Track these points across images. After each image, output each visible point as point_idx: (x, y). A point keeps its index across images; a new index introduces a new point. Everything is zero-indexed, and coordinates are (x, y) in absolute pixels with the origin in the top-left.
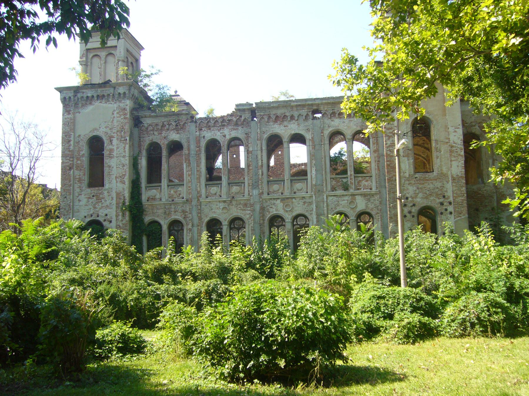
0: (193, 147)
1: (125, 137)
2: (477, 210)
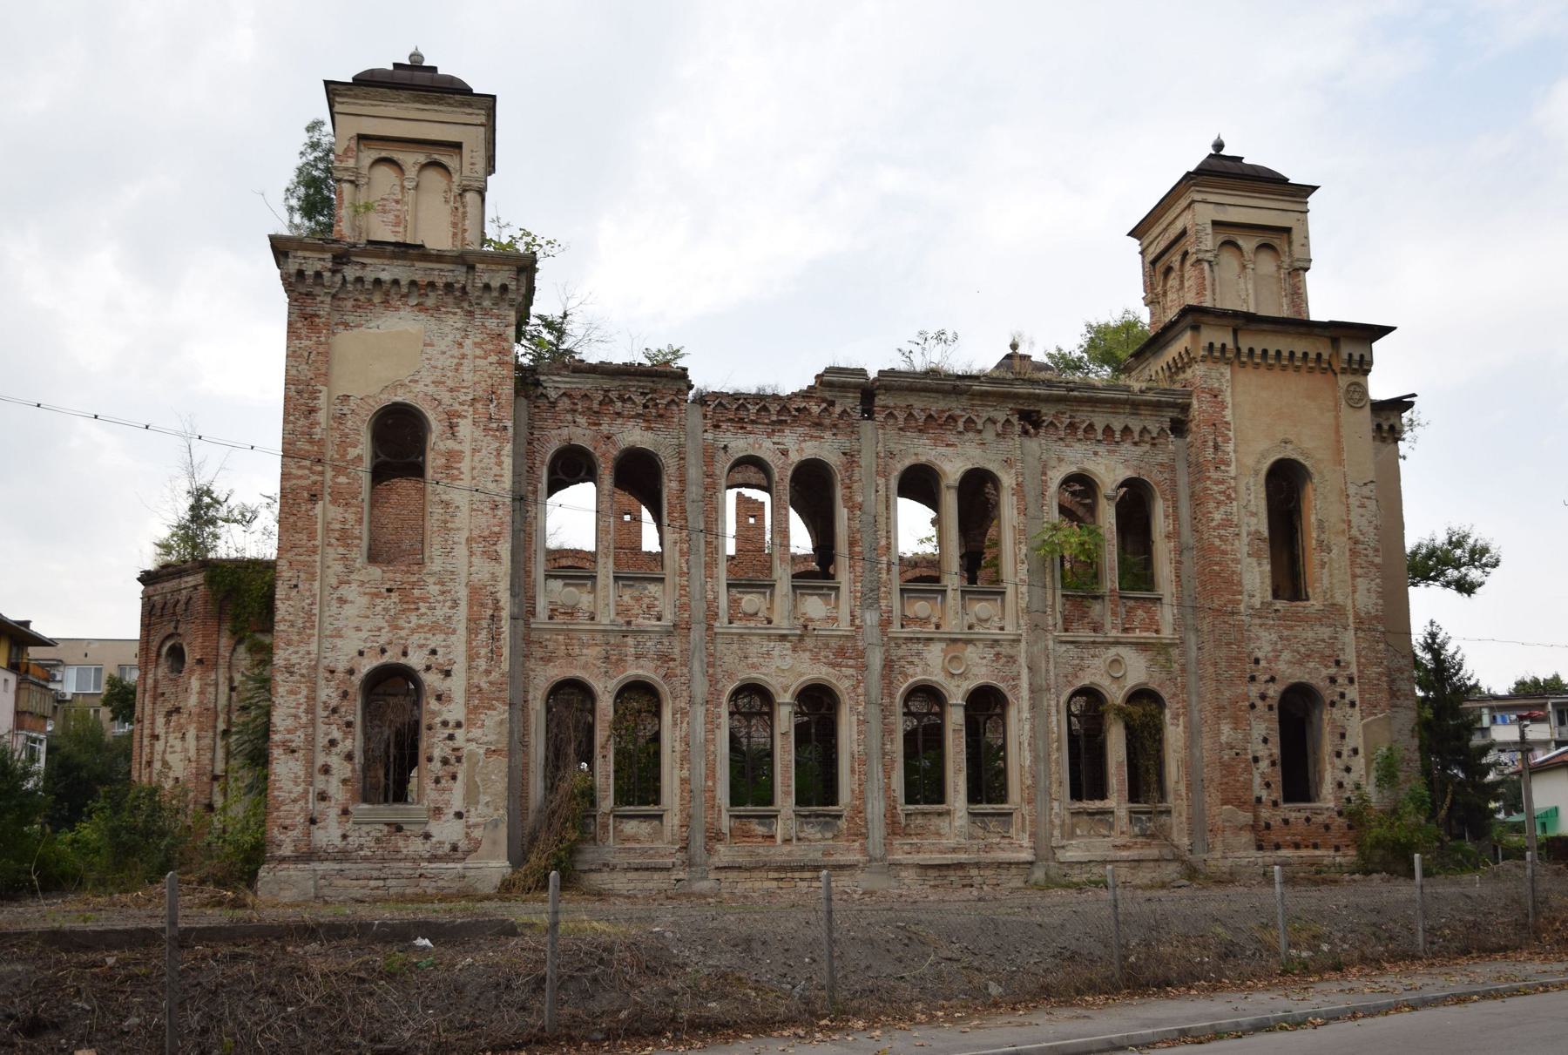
0: (694, 473)
1: (500, 420)
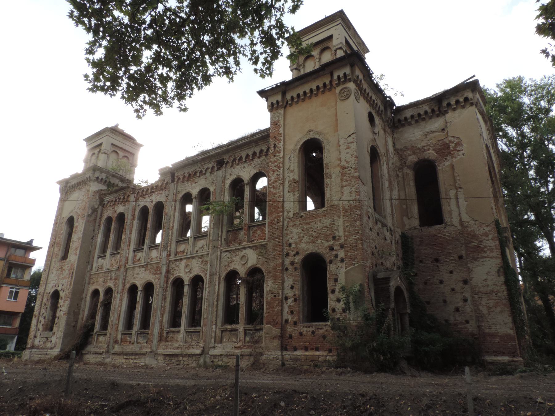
2: (437, 260)
